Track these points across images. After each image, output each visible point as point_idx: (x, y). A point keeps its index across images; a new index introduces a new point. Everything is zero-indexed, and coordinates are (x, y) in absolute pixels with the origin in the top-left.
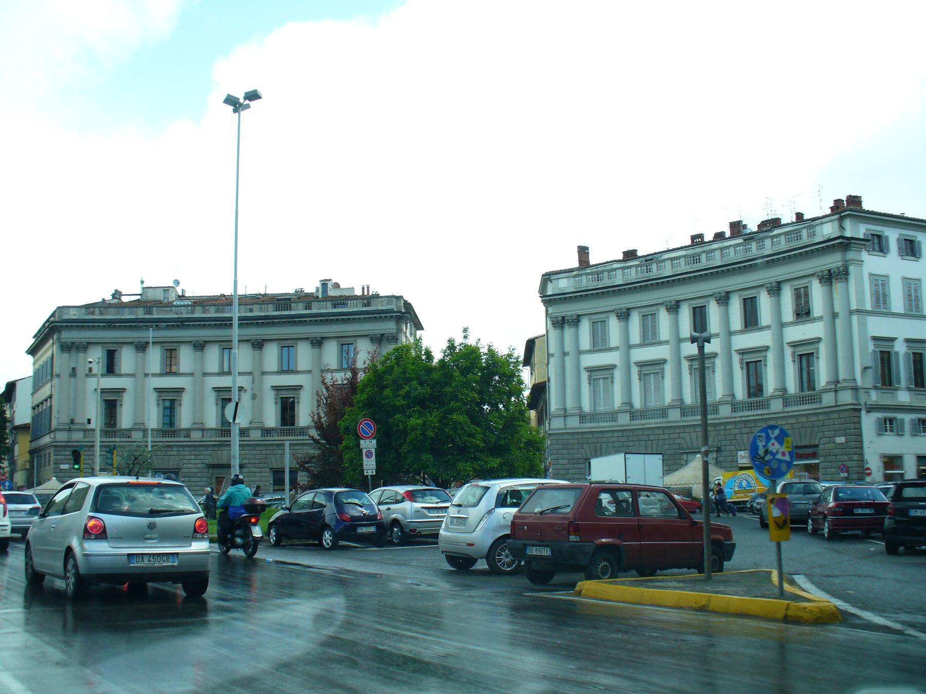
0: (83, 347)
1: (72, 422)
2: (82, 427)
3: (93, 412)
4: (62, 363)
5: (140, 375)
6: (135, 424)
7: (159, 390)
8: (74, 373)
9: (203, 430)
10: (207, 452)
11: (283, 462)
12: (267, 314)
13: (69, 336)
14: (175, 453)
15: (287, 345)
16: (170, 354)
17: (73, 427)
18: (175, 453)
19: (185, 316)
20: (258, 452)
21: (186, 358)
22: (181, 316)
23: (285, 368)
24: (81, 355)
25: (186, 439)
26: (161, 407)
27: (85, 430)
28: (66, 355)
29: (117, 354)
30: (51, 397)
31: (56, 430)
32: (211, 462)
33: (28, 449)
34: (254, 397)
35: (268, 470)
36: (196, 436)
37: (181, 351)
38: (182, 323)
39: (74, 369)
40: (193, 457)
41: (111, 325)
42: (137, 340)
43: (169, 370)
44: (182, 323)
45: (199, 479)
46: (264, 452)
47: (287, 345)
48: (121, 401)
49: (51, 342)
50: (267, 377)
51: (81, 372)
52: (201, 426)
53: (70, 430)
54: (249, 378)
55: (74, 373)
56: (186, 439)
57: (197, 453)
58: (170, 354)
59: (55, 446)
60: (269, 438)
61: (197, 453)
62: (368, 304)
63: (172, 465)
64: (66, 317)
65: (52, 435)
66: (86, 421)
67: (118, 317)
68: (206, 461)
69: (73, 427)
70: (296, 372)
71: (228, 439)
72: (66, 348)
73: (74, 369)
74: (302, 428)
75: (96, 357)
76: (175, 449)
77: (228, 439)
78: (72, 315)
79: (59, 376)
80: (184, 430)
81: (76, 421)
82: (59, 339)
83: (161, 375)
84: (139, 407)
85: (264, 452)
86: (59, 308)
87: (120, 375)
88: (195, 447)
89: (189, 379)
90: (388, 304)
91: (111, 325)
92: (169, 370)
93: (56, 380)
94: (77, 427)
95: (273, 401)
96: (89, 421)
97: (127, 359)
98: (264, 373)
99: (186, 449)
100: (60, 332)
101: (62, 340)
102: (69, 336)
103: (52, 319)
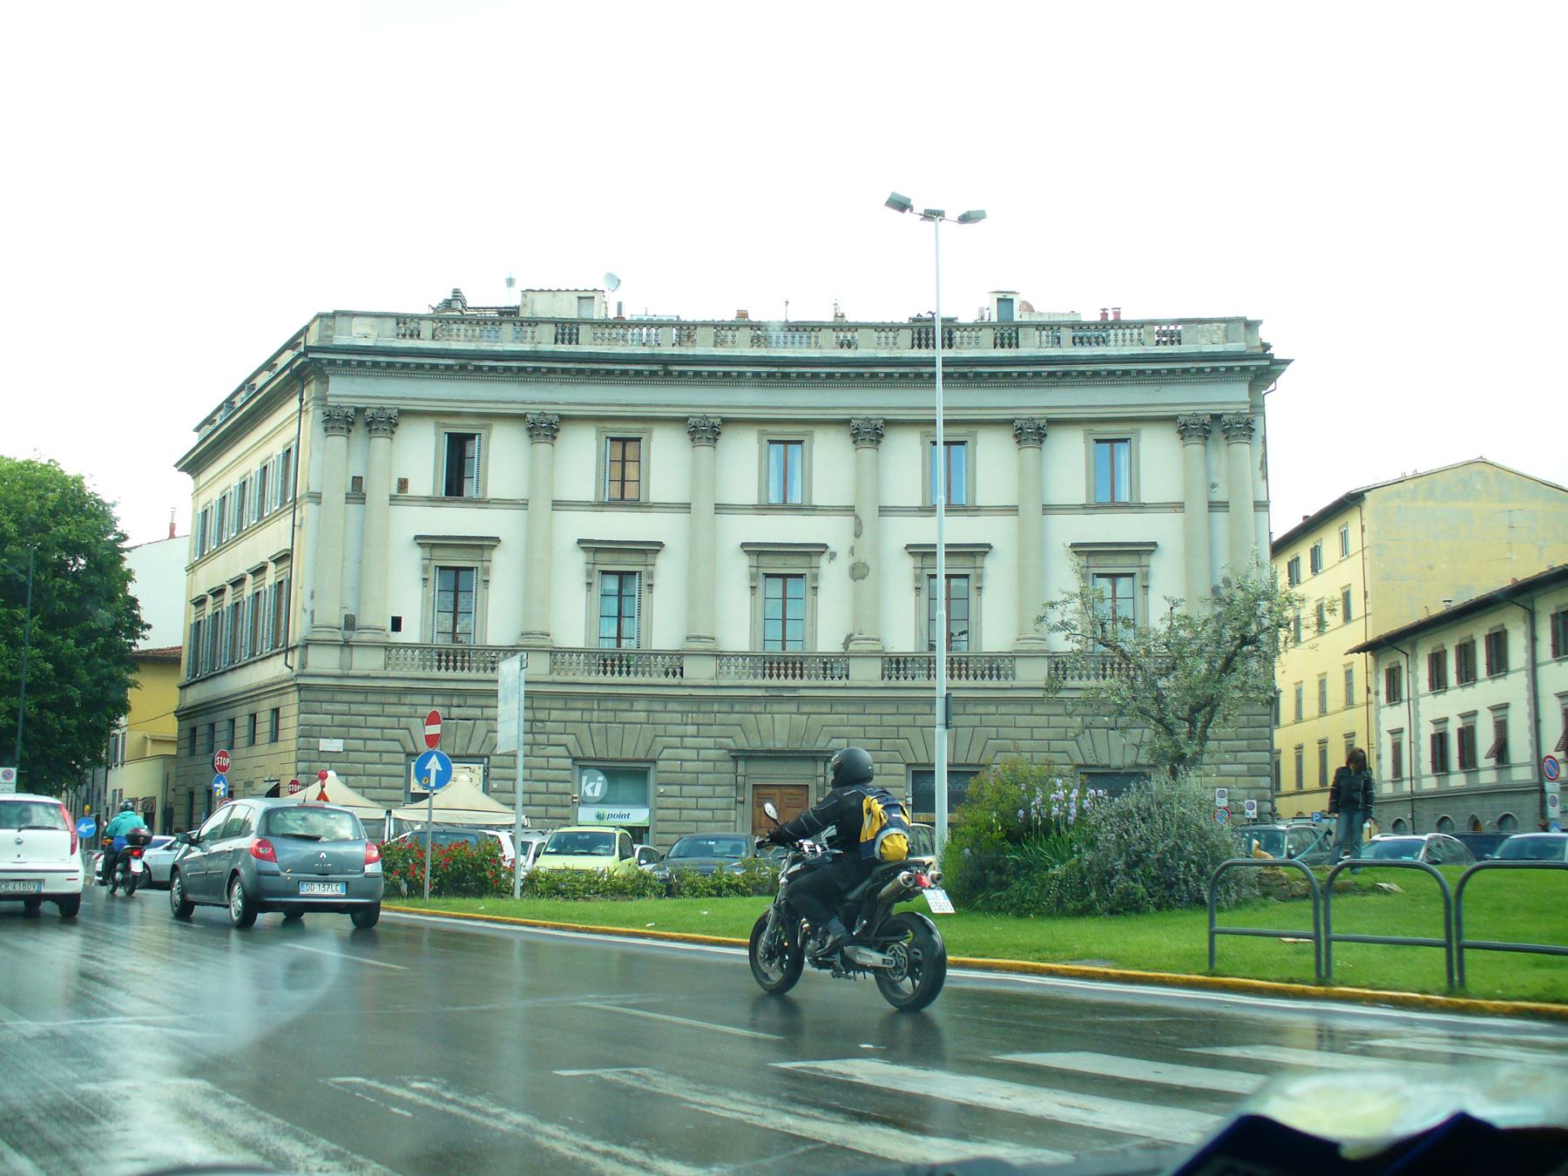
0: (382, 422)
1: (350, 623)
2: (381, 638)
3: (407, 597)
4: (324, 461)
5: (1031, 509)
6: (524, 634)
7: (428, 543)
8: (357, 491)
9: (719, 655)
10: (734, 718)
11: (929, 747)
12: (896, 353)
13: (345, 390)
14: (642, 716)
15: (1112, 436)
16: (625, 447)
17: (354, 637)
18: (642, 716)
19: (667, 350)
20: (1042, 721)
21: (667, 461)
22: (657, 351)
23: (774, 498)
24: (380, 443)
25: (671, 680)
26: (596, 592)
27: (388, 647)
28: (339, 442)
29: (472, 449)
30: (284, 558)
31: (306, 644)
32: (742, 743)
33: (174, 704)
34: (858, 572)
35: (902, 768)
36: (699, 671)
37: (1141, 444)
38: (663, 370)
39: (357, 481)
40: (691, 729)
41: (467, 366)
42: (1188, 410)
43: (623, 493)
44: (663, 370)
45: (708, 790)
46: (888, 720)
47: (1112, 436)
48: (487, 571)
49: (293, 405)
50: (728, 520)
51: (380, 488)
52: (710, 646)
53: (346, 645)
54: (847, 522)
55: (357, 491)
56: (843, 682)
57: (700, 718)
58: (625, 447)
59: (300, 688)
60: (902, 682)
61: (700, 718)
62: (1013, 342)
63: (631, 747)
64: (341, 340)
65: (295, 659)
66: (389, 625)
67: (485, 346)
68: (733, 745)
69: (354, 637)
70: (973, 510)
71: (489, 675)
72: (339, 421)
73: (357, 481)
74: (992, 658)
75: (418, 455)
76: (640, 705)
77: (489, 675)
78: (359, 334)
79: (316, 498)
80: (663, 654)
81: (360, 622)
82: (322, 399)
83: (599, 505)
84: (700, 592)
85: (888, 720)
86: (320, 316)
87: (482, 502)
88: (698, 701)
89: (1172, 521)
90: (1227, 338)
91: (467, 366)
92: (623, 493)
93: (307, 510)
94: (367, 637)
95: (910, 584)
96: (396, 624)
97: (504, 459)
98: (1048, 509)
99: (671, 706)
100: (323, 379)
101: (332, 401)
102: (345, 390)
103: (312, 340)
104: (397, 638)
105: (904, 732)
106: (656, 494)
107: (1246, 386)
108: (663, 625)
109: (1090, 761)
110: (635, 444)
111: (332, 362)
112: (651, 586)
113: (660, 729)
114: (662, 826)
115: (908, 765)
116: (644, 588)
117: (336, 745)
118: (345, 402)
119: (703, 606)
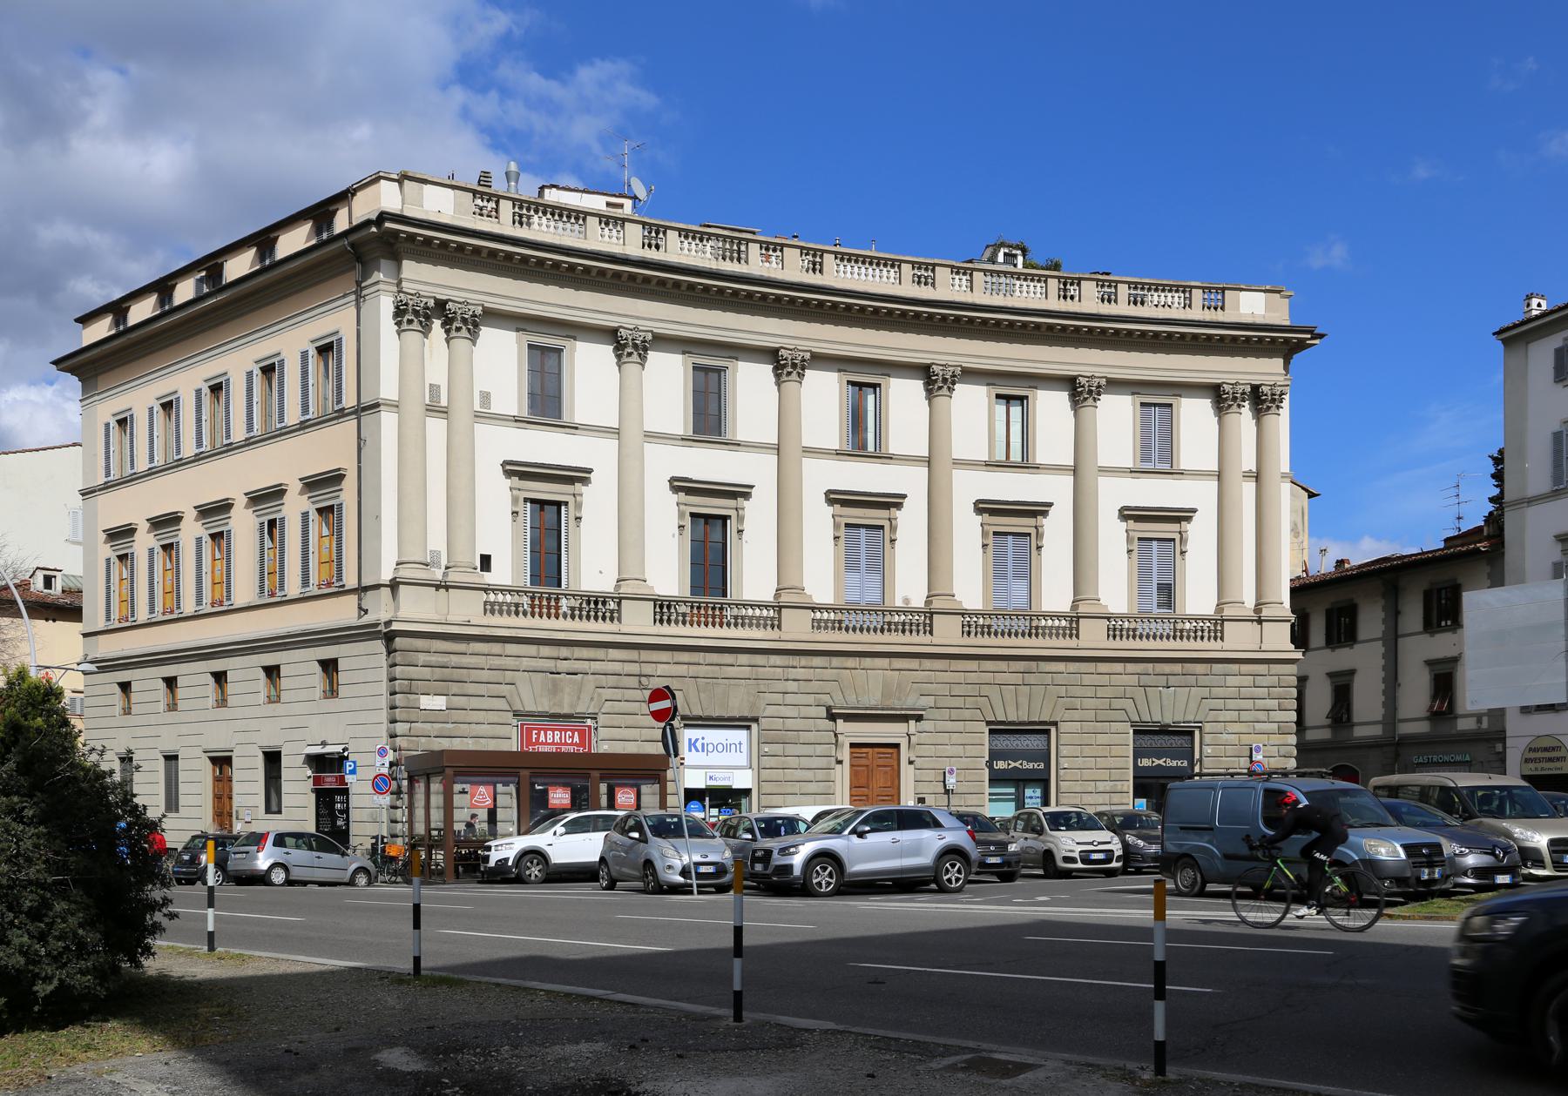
3: (501, 536)
7: (517, 471)
10: (829, 674)
31: (394, 585)
47: (1157, 397)
96: (486, 562)
98: (617, 432)
104: (489, 578)
105: (985, 690)
106: (1185, 461)
107: (1281, 361)
108: (909, 585)
109: (1001, 718)
110: (554, 356)
111: (411, 237)
112: (578, 519)
113: (763, 686)
114: (767, 788)
115: (988, 723)
116: (572, 522)
117: (439, 702)
118: (425, 290)
119: (940, 565)
